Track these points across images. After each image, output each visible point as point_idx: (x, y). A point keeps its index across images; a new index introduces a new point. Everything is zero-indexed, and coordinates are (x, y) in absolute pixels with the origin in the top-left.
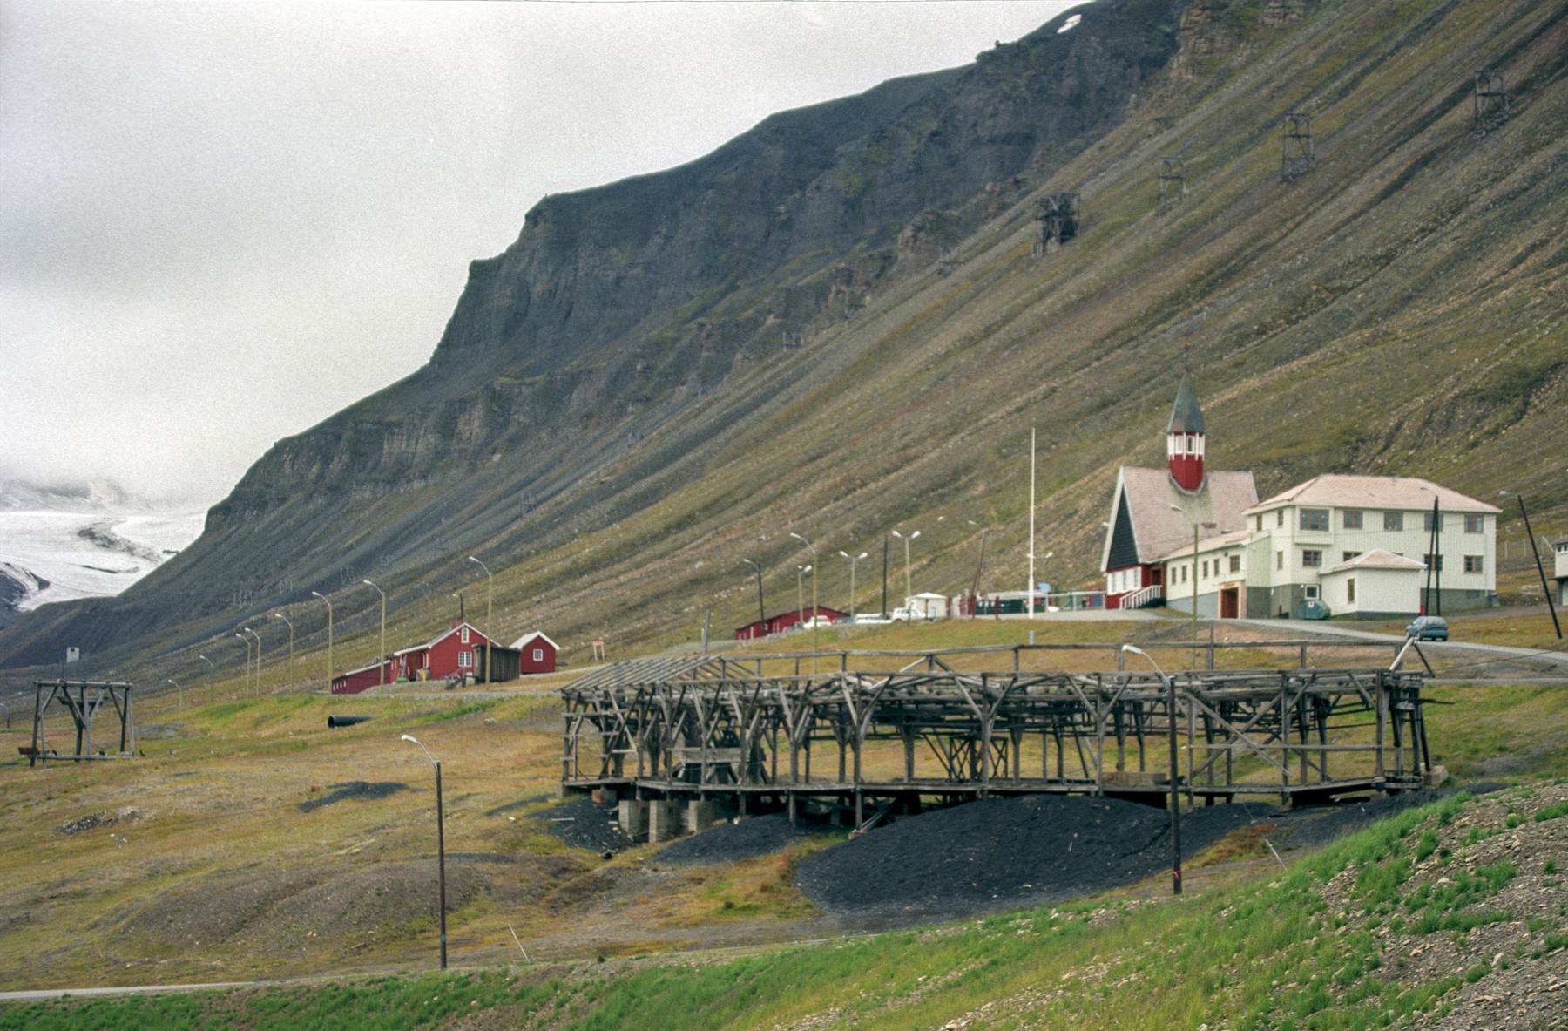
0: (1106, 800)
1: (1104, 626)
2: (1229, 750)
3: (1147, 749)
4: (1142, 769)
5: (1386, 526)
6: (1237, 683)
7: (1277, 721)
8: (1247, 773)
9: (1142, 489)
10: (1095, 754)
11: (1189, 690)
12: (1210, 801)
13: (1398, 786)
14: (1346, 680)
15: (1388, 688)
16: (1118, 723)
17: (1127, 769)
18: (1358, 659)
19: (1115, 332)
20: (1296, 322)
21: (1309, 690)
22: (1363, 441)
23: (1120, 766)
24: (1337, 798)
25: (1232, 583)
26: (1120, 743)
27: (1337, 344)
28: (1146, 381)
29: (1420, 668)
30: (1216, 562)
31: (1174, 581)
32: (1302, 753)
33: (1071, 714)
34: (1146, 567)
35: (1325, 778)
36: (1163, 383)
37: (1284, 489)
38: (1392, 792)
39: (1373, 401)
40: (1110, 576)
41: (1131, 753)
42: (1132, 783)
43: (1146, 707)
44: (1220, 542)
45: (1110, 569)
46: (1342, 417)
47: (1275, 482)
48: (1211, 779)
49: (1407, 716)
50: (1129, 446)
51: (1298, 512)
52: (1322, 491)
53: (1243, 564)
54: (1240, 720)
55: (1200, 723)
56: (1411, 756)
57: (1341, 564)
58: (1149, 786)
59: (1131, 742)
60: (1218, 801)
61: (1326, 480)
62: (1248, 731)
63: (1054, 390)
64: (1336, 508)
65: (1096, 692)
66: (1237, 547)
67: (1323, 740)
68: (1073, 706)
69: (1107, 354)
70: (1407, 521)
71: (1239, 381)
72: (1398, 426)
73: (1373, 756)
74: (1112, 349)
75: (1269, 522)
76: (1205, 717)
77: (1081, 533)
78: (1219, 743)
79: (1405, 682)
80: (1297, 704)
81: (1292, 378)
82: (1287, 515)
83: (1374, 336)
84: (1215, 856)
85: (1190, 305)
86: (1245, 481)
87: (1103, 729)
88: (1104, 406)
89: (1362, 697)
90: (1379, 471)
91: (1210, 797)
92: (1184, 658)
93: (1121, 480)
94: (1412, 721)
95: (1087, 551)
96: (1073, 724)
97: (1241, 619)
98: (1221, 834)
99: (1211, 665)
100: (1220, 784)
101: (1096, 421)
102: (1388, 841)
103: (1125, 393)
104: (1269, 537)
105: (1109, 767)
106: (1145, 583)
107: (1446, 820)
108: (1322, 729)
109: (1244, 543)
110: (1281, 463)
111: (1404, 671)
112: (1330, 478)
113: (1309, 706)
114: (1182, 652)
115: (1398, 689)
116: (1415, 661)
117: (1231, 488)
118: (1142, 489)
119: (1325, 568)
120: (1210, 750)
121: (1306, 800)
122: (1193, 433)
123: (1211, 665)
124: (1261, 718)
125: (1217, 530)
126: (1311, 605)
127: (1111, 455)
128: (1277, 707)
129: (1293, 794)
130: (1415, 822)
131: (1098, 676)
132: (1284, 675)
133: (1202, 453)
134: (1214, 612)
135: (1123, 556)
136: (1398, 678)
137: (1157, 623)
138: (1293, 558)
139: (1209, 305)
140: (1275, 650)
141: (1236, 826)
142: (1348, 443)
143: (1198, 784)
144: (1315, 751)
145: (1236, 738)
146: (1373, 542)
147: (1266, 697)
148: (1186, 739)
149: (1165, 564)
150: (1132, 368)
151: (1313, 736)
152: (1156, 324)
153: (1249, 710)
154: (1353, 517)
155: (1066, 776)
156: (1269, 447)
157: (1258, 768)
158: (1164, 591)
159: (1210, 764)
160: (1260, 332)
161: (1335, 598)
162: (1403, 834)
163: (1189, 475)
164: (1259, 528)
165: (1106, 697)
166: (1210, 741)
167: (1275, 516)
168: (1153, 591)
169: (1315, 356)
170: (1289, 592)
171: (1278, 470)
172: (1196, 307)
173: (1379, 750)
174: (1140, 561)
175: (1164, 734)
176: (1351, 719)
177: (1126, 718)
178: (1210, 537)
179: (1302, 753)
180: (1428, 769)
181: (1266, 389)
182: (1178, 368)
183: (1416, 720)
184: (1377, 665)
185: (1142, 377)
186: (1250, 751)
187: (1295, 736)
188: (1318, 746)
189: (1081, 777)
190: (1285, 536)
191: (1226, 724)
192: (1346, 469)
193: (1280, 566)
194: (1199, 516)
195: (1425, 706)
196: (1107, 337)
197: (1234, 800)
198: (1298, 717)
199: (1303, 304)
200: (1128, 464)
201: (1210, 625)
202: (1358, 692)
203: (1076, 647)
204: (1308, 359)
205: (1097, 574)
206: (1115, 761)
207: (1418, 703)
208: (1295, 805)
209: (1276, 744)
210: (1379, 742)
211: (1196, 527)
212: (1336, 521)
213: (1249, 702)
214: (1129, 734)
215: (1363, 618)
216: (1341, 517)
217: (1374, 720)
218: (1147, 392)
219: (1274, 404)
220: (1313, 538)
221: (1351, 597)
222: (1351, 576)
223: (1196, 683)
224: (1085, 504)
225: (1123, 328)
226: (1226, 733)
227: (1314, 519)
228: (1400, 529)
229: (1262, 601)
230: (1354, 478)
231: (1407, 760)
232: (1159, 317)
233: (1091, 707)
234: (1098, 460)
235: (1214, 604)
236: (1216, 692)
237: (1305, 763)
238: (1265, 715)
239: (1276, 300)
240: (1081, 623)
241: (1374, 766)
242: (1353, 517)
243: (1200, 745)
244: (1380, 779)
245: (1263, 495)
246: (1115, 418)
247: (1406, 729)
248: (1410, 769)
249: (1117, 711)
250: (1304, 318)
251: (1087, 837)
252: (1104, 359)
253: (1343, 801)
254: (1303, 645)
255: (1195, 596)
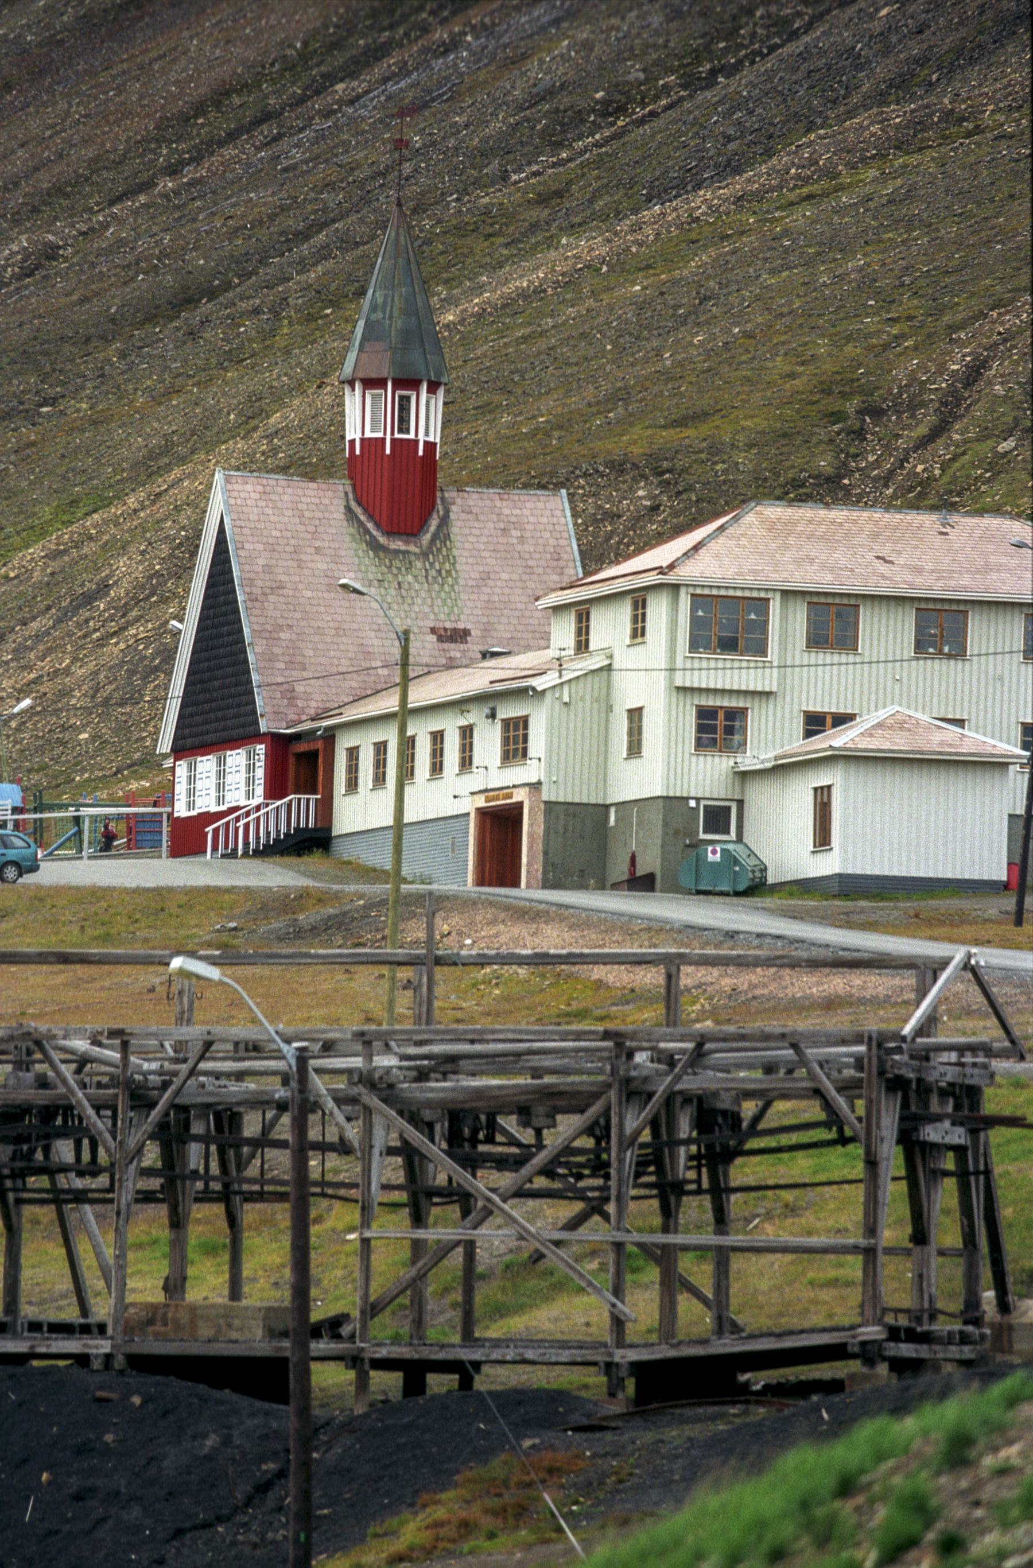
0: (134, 1379)
1: (158, 901)
2: (470, 1246)
3: (250, 1240)
4: (235, 1291)
5: (920, 647)
6: (497, 1063)
7: (600, 1167)
8: (520, 1309)
9: (273, 525)
10: (110, 1253)
11: (368, 1080)
12: (414, 1385)
13: (922, 1351)
14: (787, 1063)
15: (897, 1084)
16: (171, 1167)
17: (194, 1295)
18: (830, 1004)
19: (221, 95)
20: (710, 81)
21: (690, 1083)
22: (877, 413)
23: (174, 1286)
24: (758, 1380)
25: (506, 790)
26: (177, 1223)
27: (816, 144)
28: (304, 236)
29: (988, 1031)
30: (467, 732)
31: (352, 785)
32: (664, 1257)
33: (47, 1138)
34: (280, 746)
35: (724, 1325)
36: (347, 243)
37: (661, 538)
38: (900, 1366)
39: (908, 302)
40: (182, 769)
41: (210, 1250)
42: (205, 1331)
43: (251, 1126)
44: (477, 680)
45: (180, 751)
46: (822, 347)
47: (637, 520)
48: (419, 1323)
49: (949, 1163)
50: (253, 412)
51: (685, 602)
52: (746, 548)
53: (537, 742)
54: (501, 1163)
55: (393, 1169)
56: (954, 1271)
57: (794, 743)
58: (253, 1340)
59: (206, 1220)
60: (438, 1383)
61: (762, 518)
62: (520, 1194)
63: (51, 253)
64: (786, 594)
65: (114, 1081)
66: (522, 693)
67: (721, 1220)
68: (54, 1117)
69: (196, 161)
70: (979, 632)
71: (551, 242)
72: (974, 373)
73: (854, 1267)
74: (212, 145)
75: (610, 628)
76: (408, 1153)
77: (115, 648)
78: (443, 1227)
79: (944, 1069)
80: (654, 1124)
81: (692, 235)
82: (658, 610)
83: (918, 125)
84: (424, 1537)
85: (425, 30)
86: (549, 517)
87: (132, 1183)
88: (189, 301)
89: (828, 1106)
90: (920, 495)
91: (414, 1373)
92: (368, 995)
93: (217, 505)
94: (963, 1175)
95: (133, 699)
96: (51, 1171)
97: (528, 890)
98: (441, 1478)
99: (426, 1012)
100: (442, 1333)
101: (166, 335)
102: (804, 1505)
103: (244, 266)
104: (609, 668)
105: (146, 1287)
106: (275, 789)
107: (959, 1452)
108: (719, 1192)
109: (539, 683)
110: (659, 468)
111: (941, 1039)
112: (775, 511)
113: (685, 1127)
114: (365, 975)
115: (924, 1089)
116: (968, 1012)
117: (511, 534)
118: (273, 525)
119: (758, 753)
120: (417, 1247)
121: (673, 1384)
122: (413, 384)
123: (426, 1012)
124: (555, 1161)
125: (474, 647)
126: (713, 856)
127: (201, 440)
128: (599, 1130)
129: (639, 1368)
130: (880, 1457)
131: (122, 1038)
132: (622, 1045)
133: (434, 437)
134: (459, 873)
135: (217, 714)
136: (924, 1056)
137: (303, 895)
138: (668, 728)
139: (482, 30)
140: (614, 976)
141: (483, 1456)
142: (837, 416)
143: (385, 1338)
144: (701, 1249)
145: (488, 1213)
146: (884, 688)
147: (573, 1101)
148: (353, 1215)
149: (330, 737)
150: (264, 198)
151: (695, 1209)
152: (331, 78)
153: (527, 1136)
154: (834, 621)
155: (28, 1311)
156: (626, 422)
157: (547, 1297)
158: (326, 808)
159: (422, 1276)
160: (610, 109)
161: (782, 837)
162: (846, 1487)
163: (400, 498)
164: (582, 646)
165: (140, 1098)
166: (418, 1219)
167: (624, 612)
168: (298, 809)
169: (757, 176)
170: (656, 817)
171: (643, 487)
172: (440, 34)
173: (869, 1253)
174: (263, 729)
175: (282, 1197)
176: (801, 1166)
177: (194, 1154)
178: (451, 665)
179: (664, 1257)
180: (1004, 1307)
181: (622, 266)
182: (386, 199)
183: (974, 1174)
184: (872, 1025)
185: (293, 222)
186: (529, 1247)
187: (646, 1210)
188: (709, 1238)
189: (71, 1314)
190: (649, 667)
191: (463, 1177)
192: (829, 489)
193: (635, 748)
194: (423, 609)
195: (996, 1136)
196: (200, 109)
197: (480, 1384)
198: (655, 1158)
199: (732, 33)
200: (248, 465)
201: (434, 904)
202: (818, 1093)
203: (65, 959)
204: (738, 184)
205: (150, 762)
206: (163, 1268)
207: (979, 1124)
208: (642, 1398)
209: (595, 1231)
210: (871, 1229)
211: (405, 638)
212: (787, 628)
213: (524, 1113)
214: (205, 1197)
215: (852, 893)
216: (799, 618)
217: (859, 1170)
218: (303, 266)
219: (640, 307)
220: (727, 674)
221: (823, 838)
222: (822, 778)
223: (385, 1061)
224: (127, 570)
225: (243, 88)
226: (464, 1199)
227: (728, 624)
228: (959, 653)
229: (587, 841)
230: (839, 514)
231: (946, 1279)
232: (339, 59)
233: (100, 1125)
234: (167, 448)
235: (457, 846)
236: (438, 1087)
237: (672, 1283)
238: (568, 1150)
239: (656, 20)
240: (97, 893)
241: (855, 1296)
242: (834, 621)
243: (392, 1230)
244: (872, 1332)
245: (595, 555)
246: (214, 335)
247: (946, 1195)
248: (955, 1306)
249: (172, 1135)
250: (731, 71)
251: (74, 1483)
252: (189, 173)
253: (776, 1391)
254: (672, 964)
255: (399, 825)
